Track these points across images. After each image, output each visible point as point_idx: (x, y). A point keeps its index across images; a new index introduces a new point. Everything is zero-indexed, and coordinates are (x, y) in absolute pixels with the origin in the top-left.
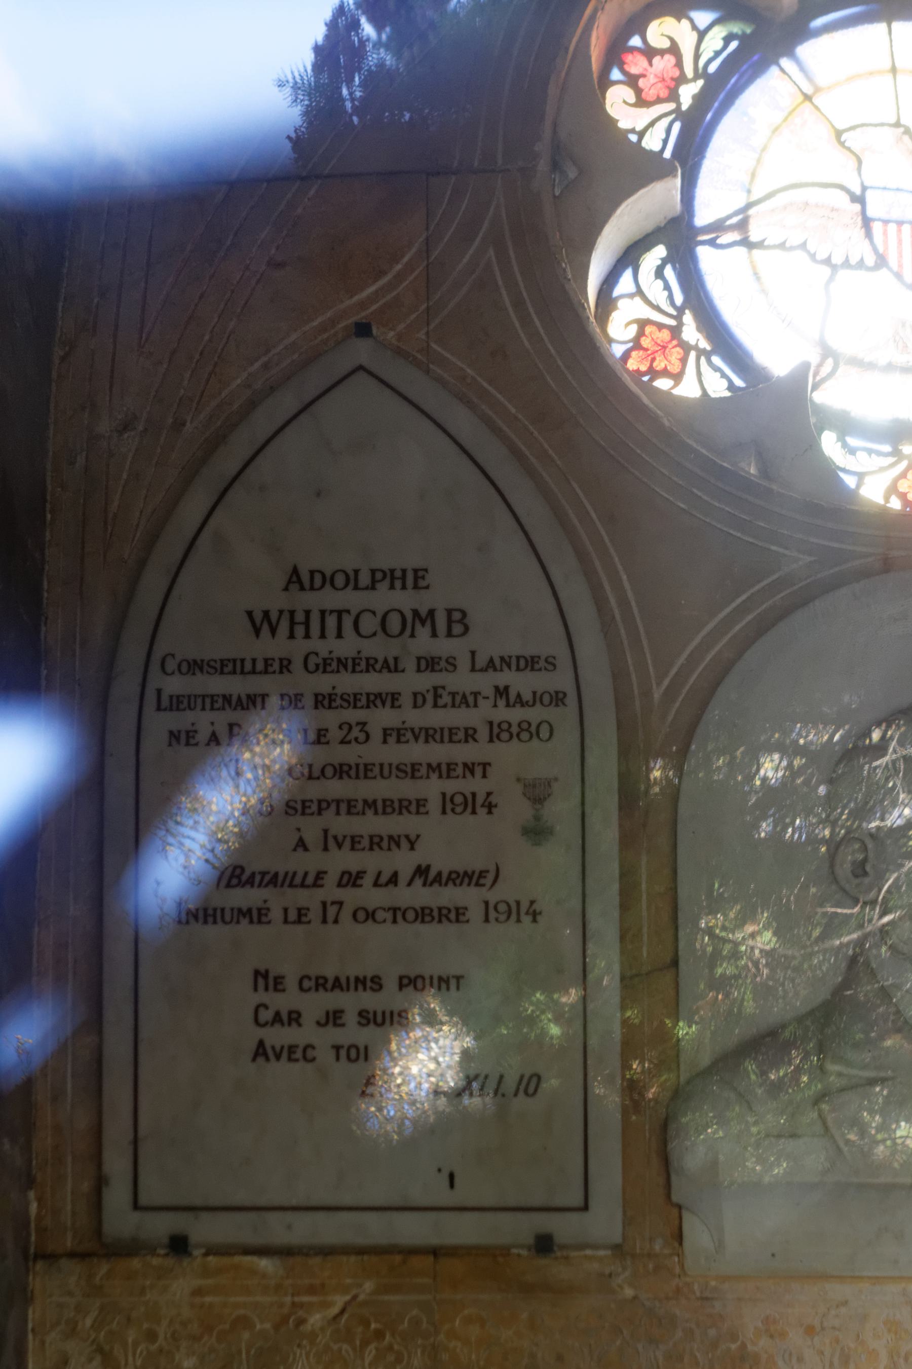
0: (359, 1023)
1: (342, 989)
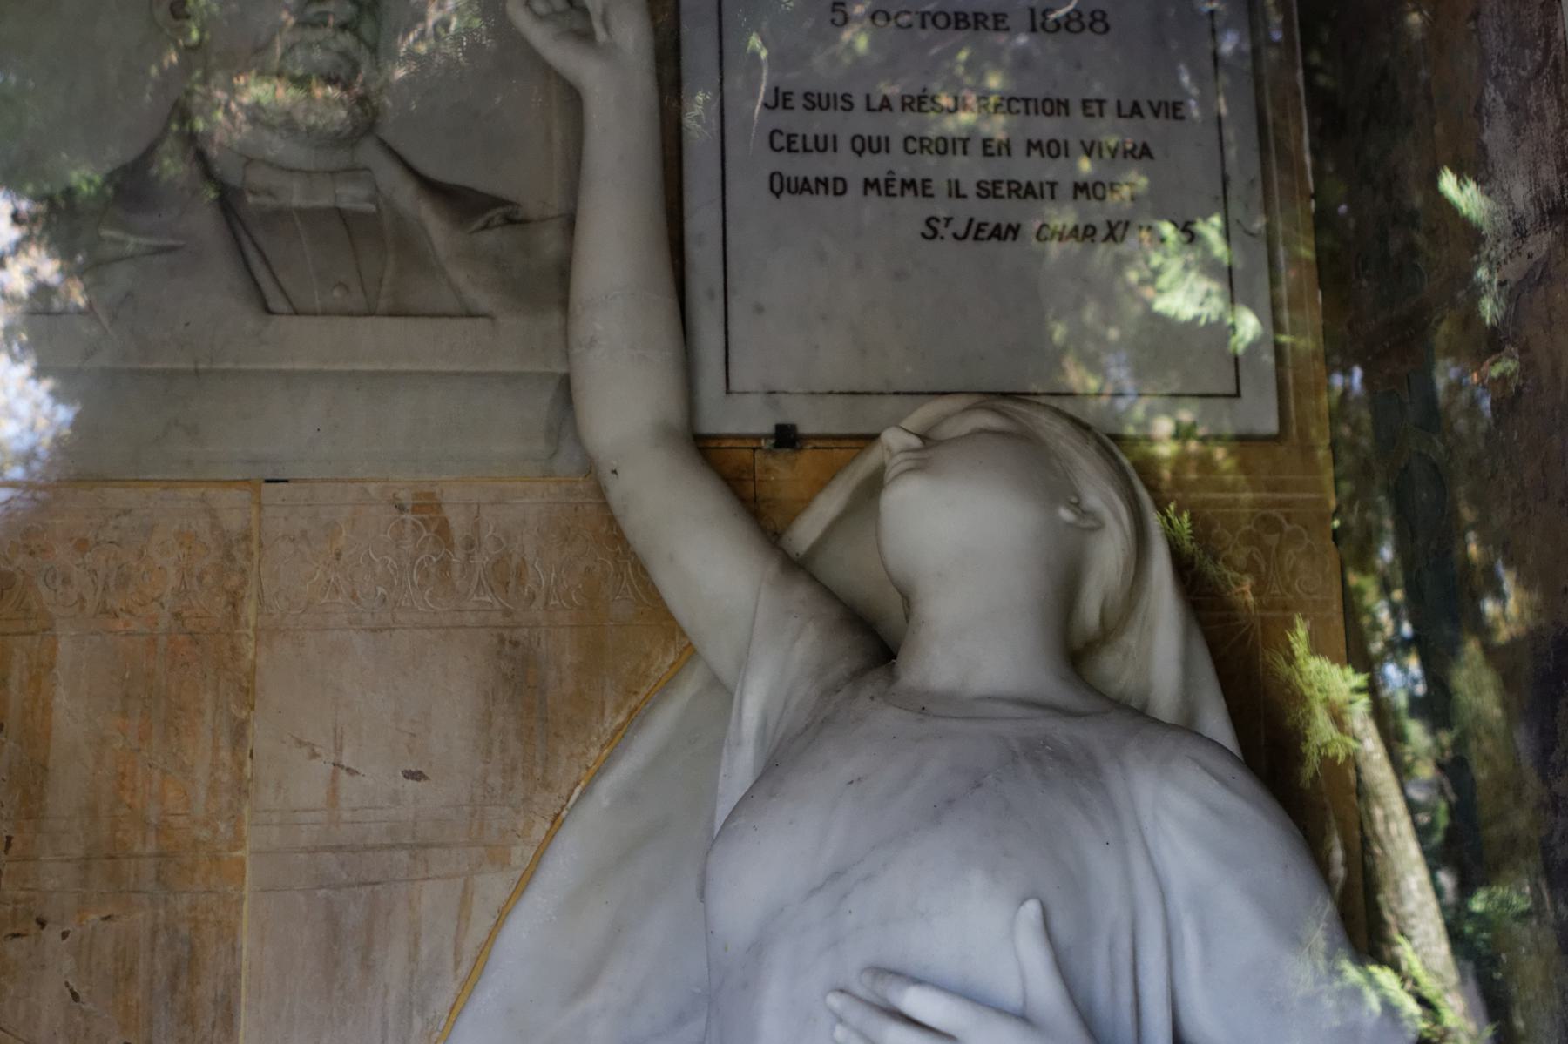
0: (979, 195)
1: (1035, 197)
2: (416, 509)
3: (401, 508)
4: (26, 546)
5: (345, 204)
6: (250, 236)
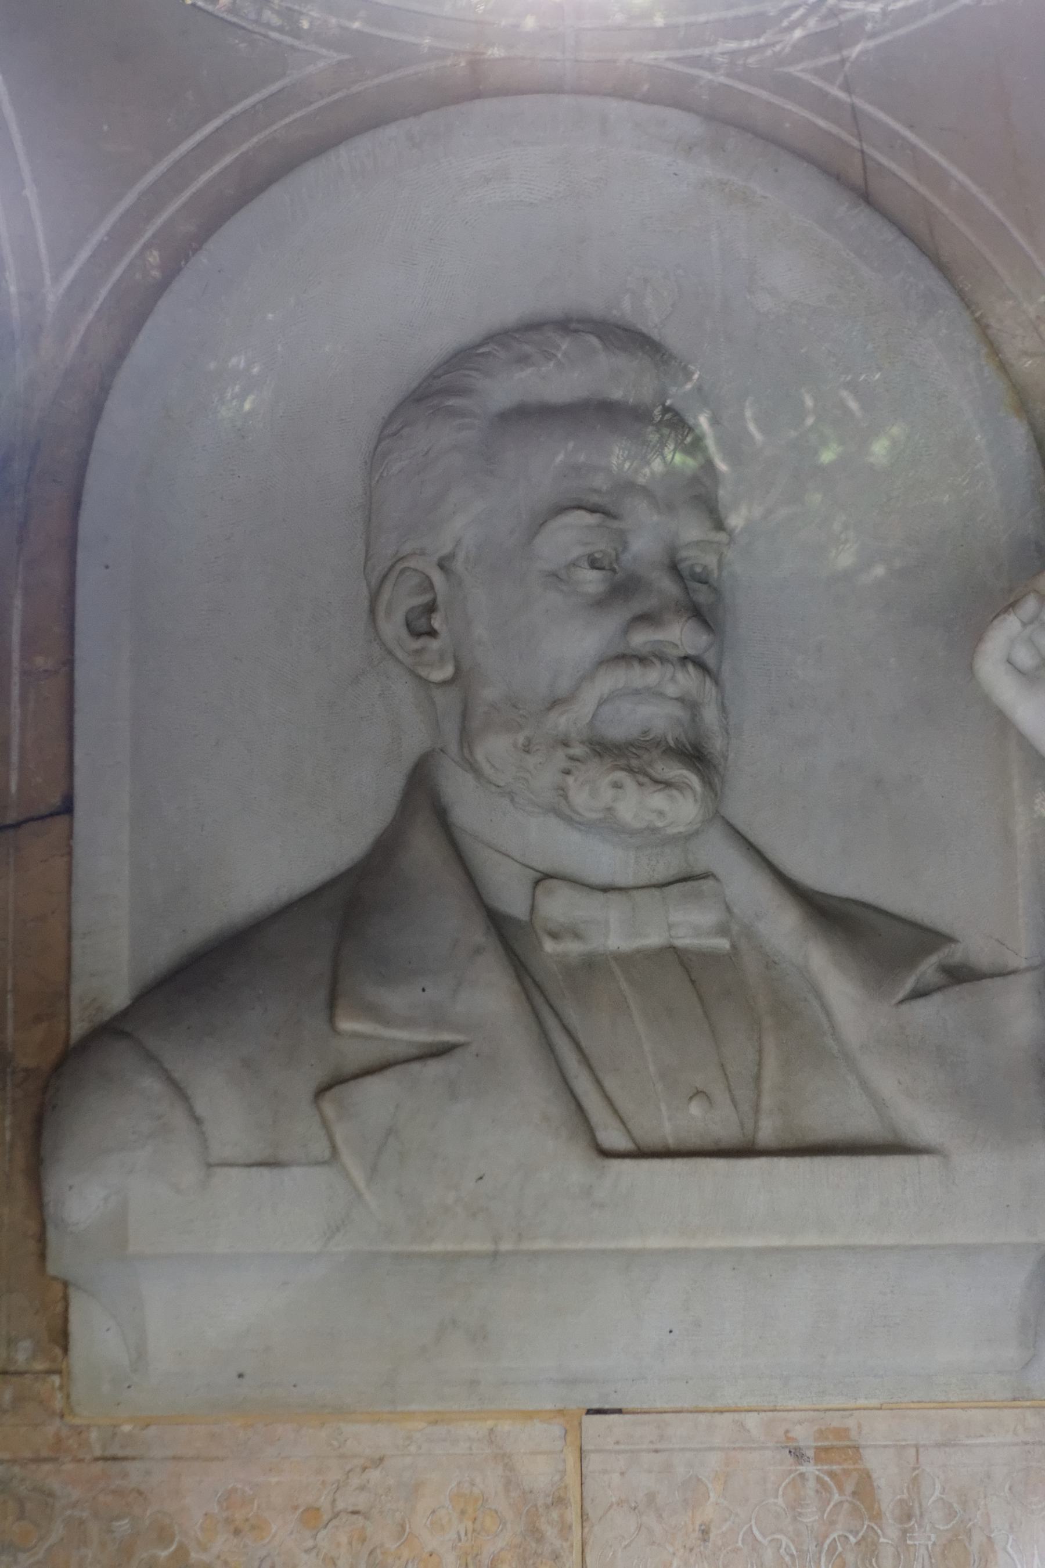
2: (823, 1453)
3: (798, 1454)
4: (228, 1521)
5: (685, 940)
6: (557, 1014)
